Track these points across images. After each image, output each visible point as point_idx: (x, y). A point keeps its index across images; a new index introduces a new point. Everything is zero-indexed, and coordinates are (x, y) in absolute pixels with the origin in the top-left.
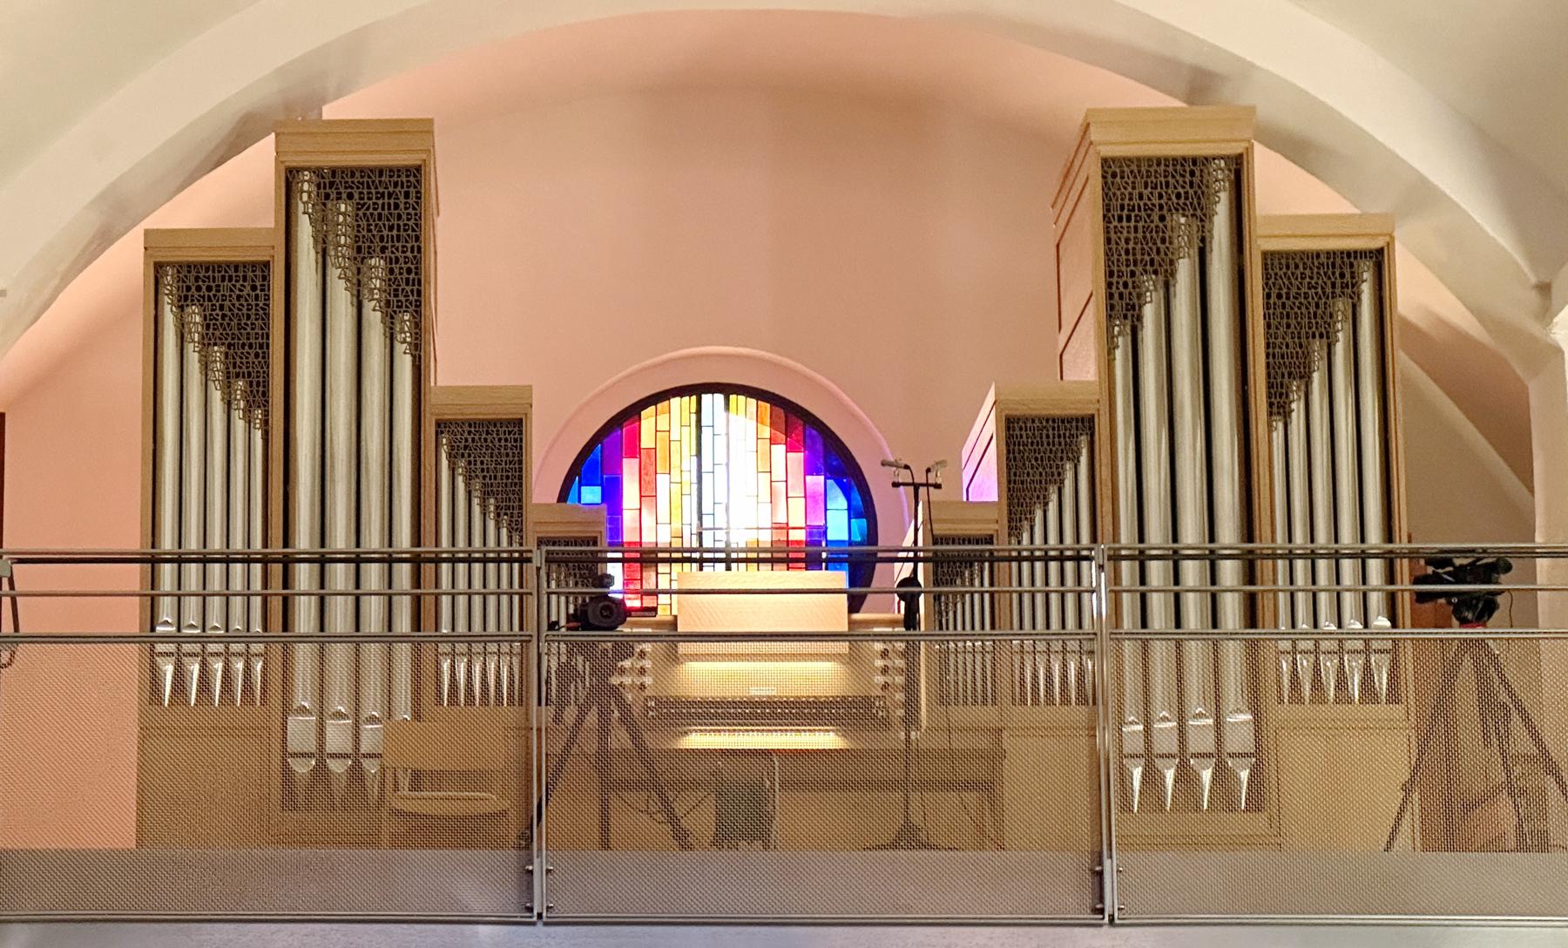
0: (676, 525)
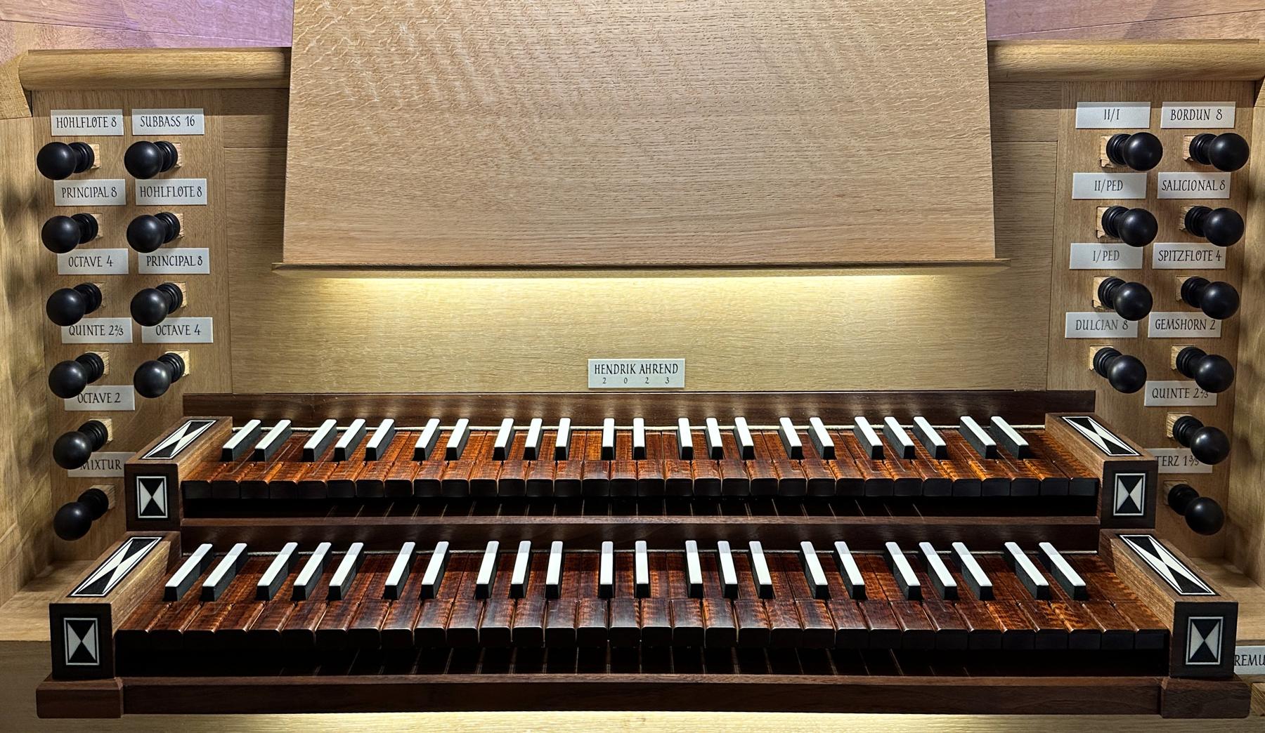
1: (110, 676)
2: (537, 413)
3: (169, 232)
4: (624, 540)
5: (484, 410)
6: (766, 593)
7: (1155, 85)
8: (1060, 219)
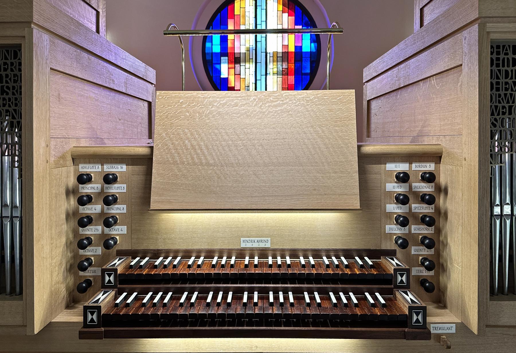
1: (100, 327)
2: (225, 255)
3: (115, 200)
4: (251, 291)
5: (209, 254)
6: (292, 305)
7: (410, 157)
8: (383, 197)
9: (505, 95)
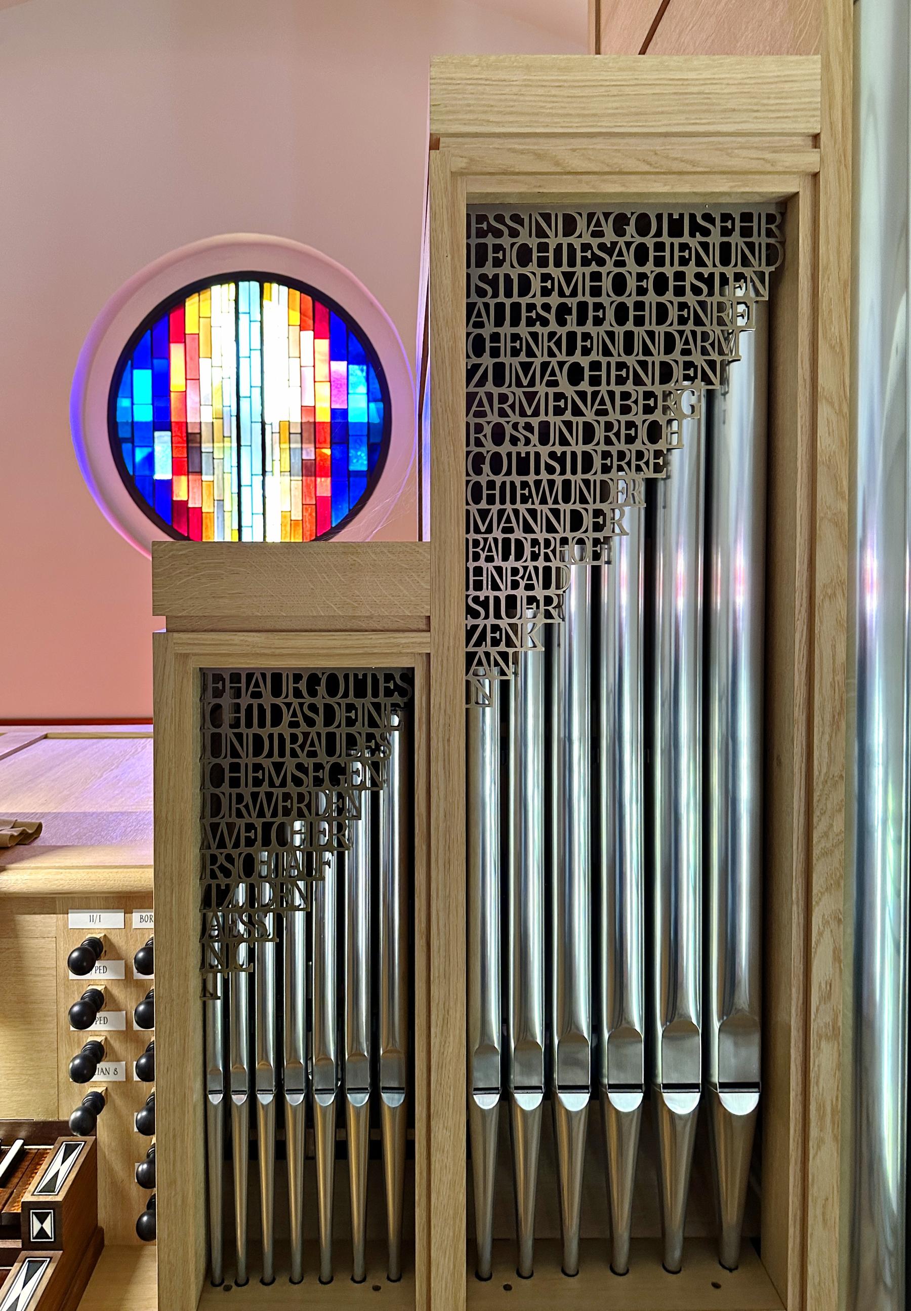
0: (218, 406)
9: (255, 796)
